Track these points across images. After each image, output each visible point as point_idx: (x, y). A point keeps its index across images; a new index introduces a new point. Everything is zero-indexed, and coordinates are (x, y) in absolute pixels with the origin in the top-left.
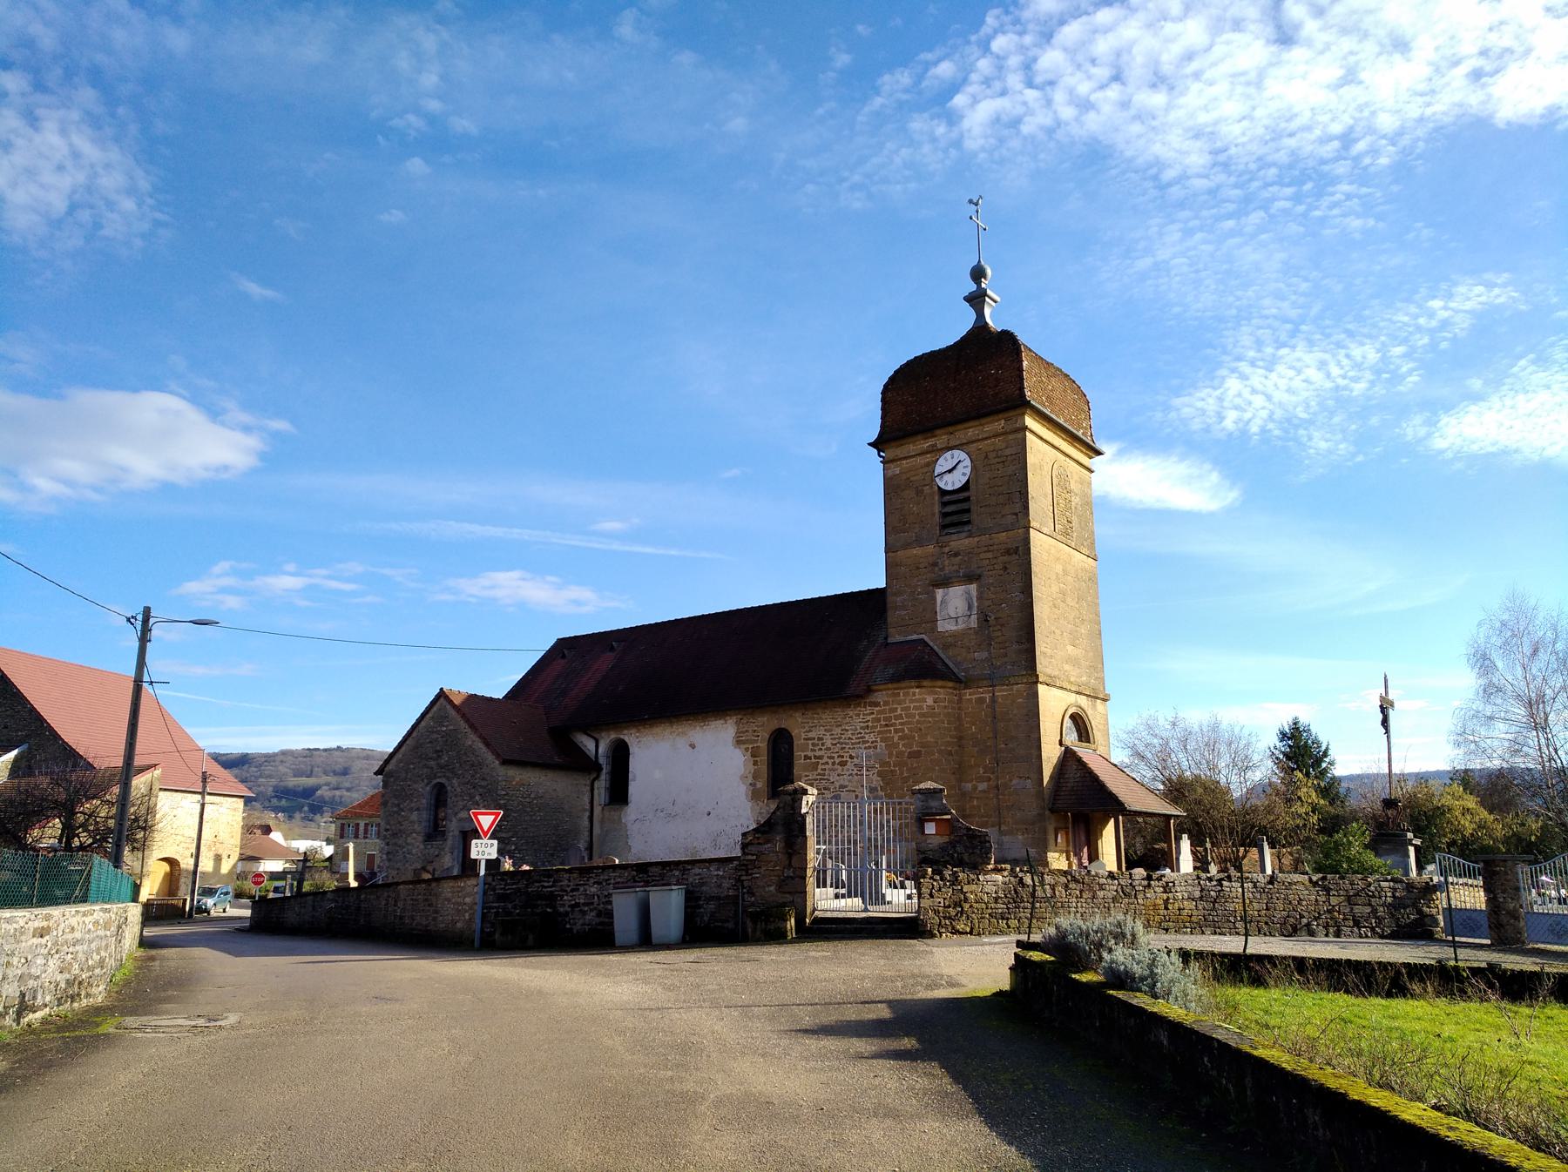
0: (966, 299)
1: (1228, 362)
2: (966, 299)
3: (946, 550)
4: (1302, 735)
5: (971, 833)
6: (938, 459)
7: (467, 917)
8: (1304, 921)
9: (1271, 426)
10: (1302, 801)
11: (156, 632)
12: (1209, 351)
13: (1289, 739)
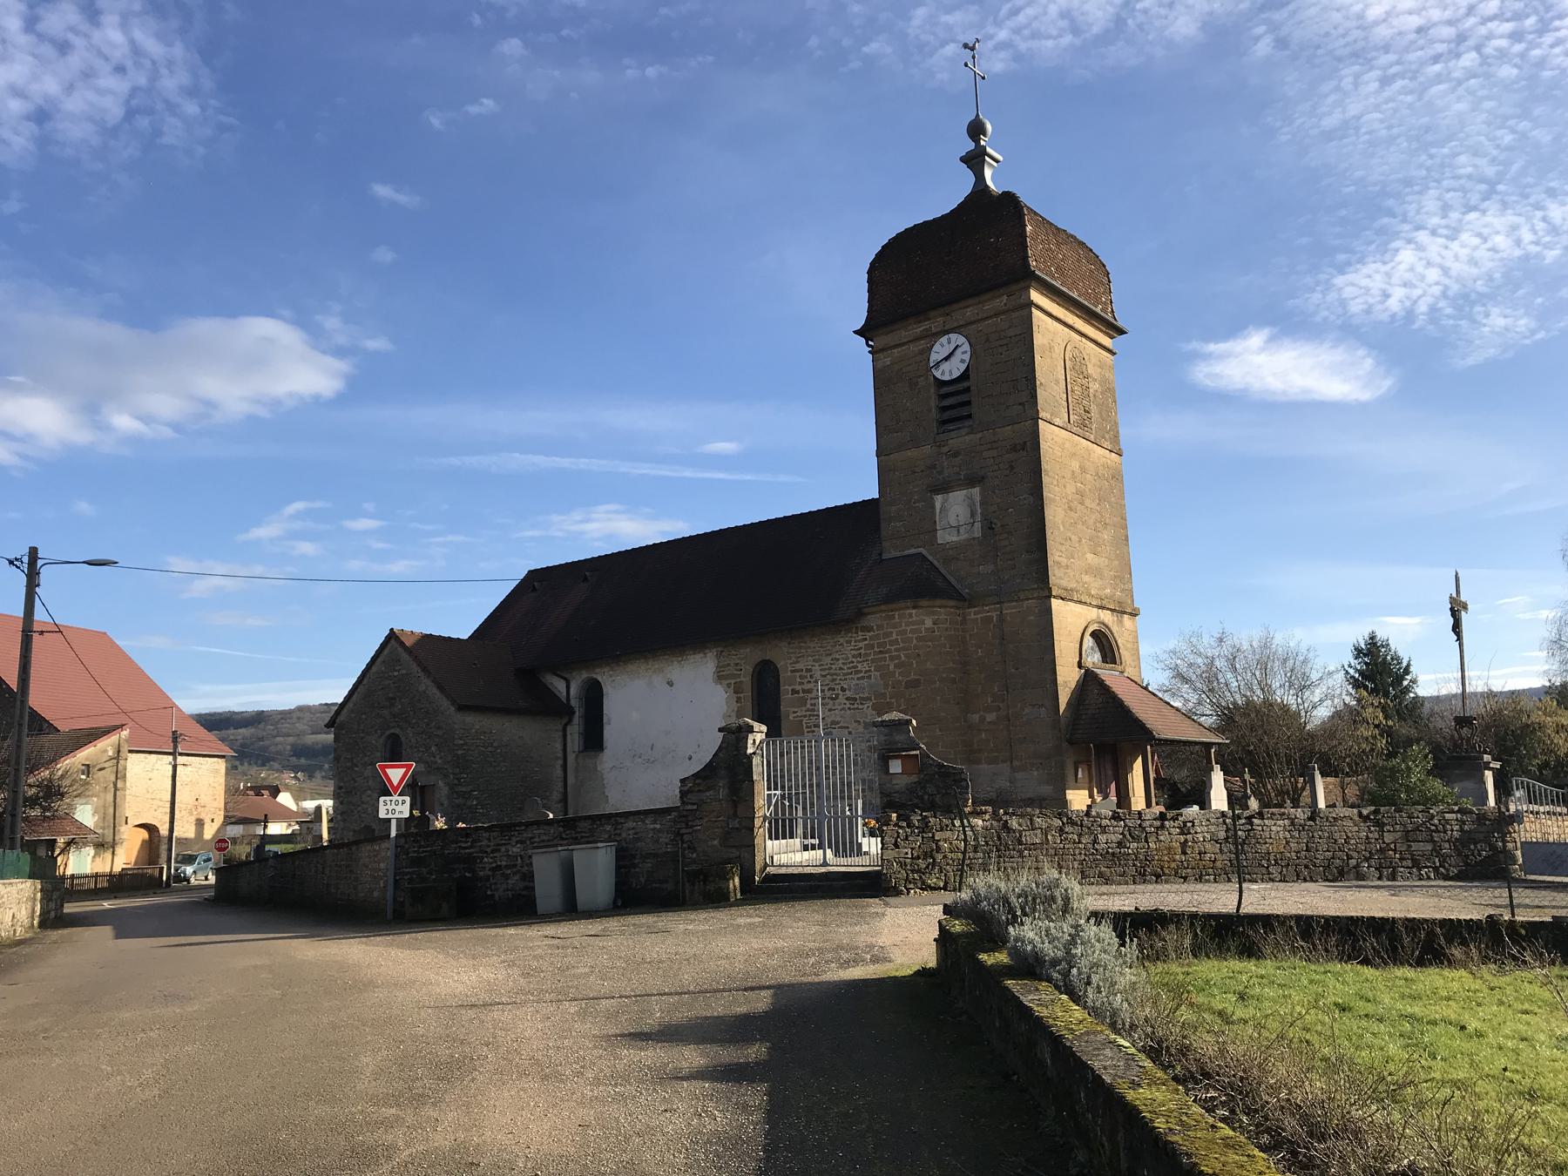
0: (963, 160)
1: (1407, 232)
2: (963, 160)
3: (945, 449)
4: (1380, 651)
5: (943, 770)
6: (933, 345)
7: (382, 885)
8: (1353, 862)
9: (1442, 304)
10: (1368, 723)
11: (46, 574)
12: (1386, 220)
13: (1365, 655)
